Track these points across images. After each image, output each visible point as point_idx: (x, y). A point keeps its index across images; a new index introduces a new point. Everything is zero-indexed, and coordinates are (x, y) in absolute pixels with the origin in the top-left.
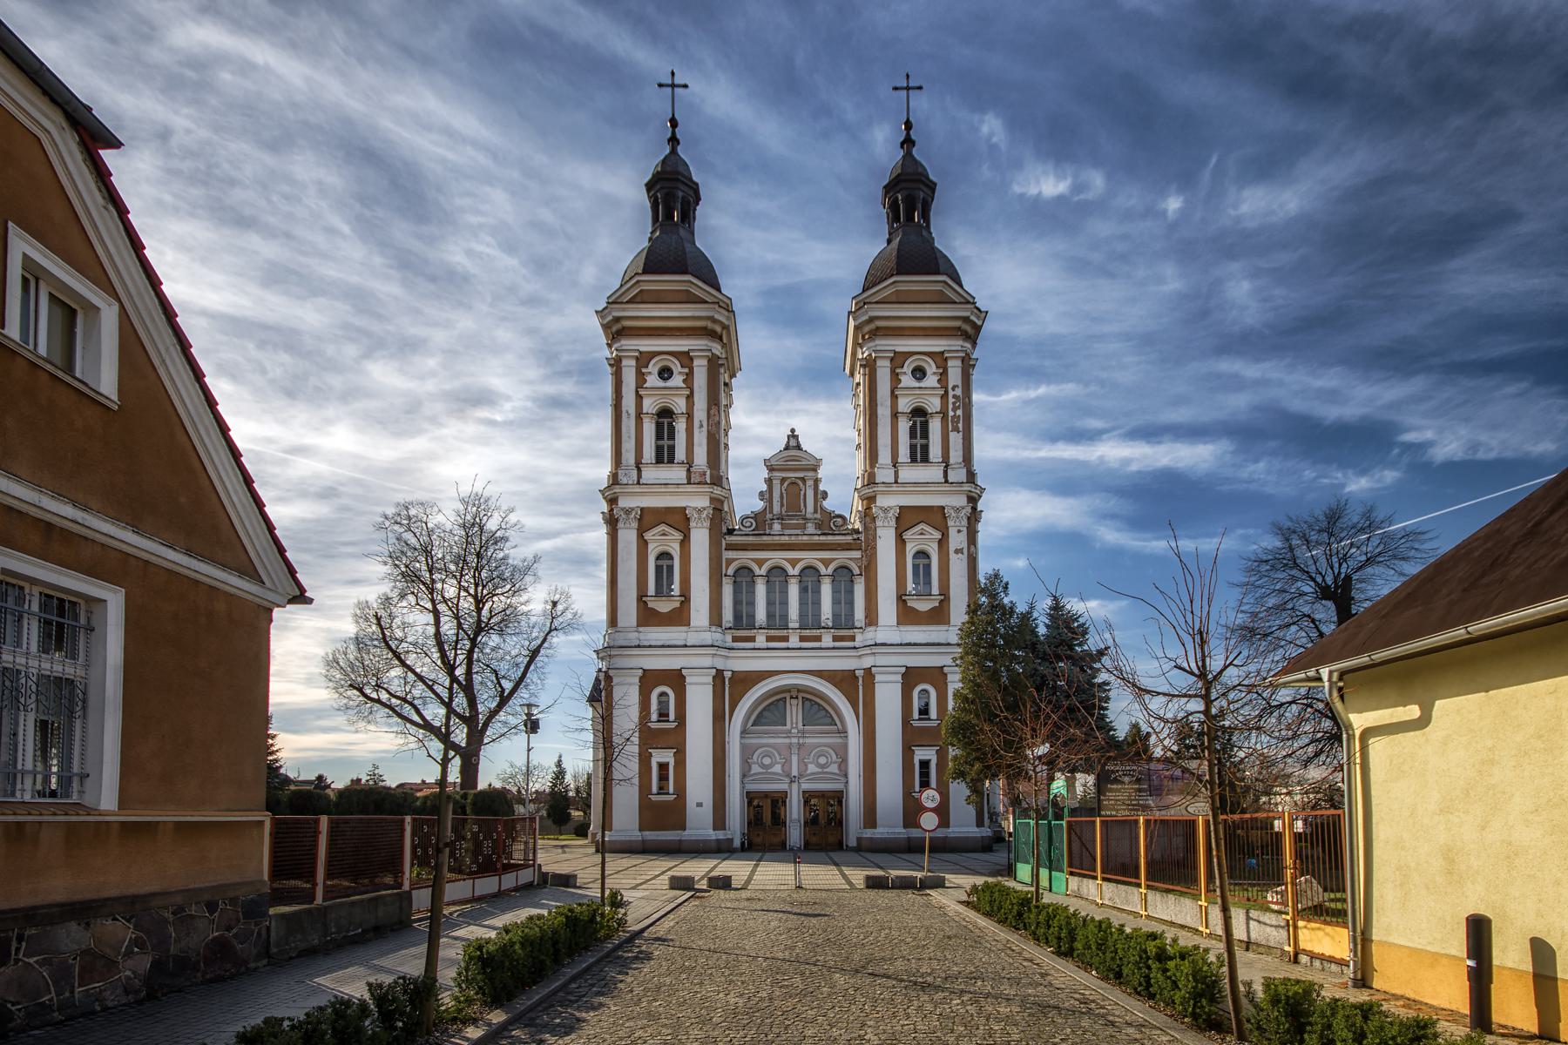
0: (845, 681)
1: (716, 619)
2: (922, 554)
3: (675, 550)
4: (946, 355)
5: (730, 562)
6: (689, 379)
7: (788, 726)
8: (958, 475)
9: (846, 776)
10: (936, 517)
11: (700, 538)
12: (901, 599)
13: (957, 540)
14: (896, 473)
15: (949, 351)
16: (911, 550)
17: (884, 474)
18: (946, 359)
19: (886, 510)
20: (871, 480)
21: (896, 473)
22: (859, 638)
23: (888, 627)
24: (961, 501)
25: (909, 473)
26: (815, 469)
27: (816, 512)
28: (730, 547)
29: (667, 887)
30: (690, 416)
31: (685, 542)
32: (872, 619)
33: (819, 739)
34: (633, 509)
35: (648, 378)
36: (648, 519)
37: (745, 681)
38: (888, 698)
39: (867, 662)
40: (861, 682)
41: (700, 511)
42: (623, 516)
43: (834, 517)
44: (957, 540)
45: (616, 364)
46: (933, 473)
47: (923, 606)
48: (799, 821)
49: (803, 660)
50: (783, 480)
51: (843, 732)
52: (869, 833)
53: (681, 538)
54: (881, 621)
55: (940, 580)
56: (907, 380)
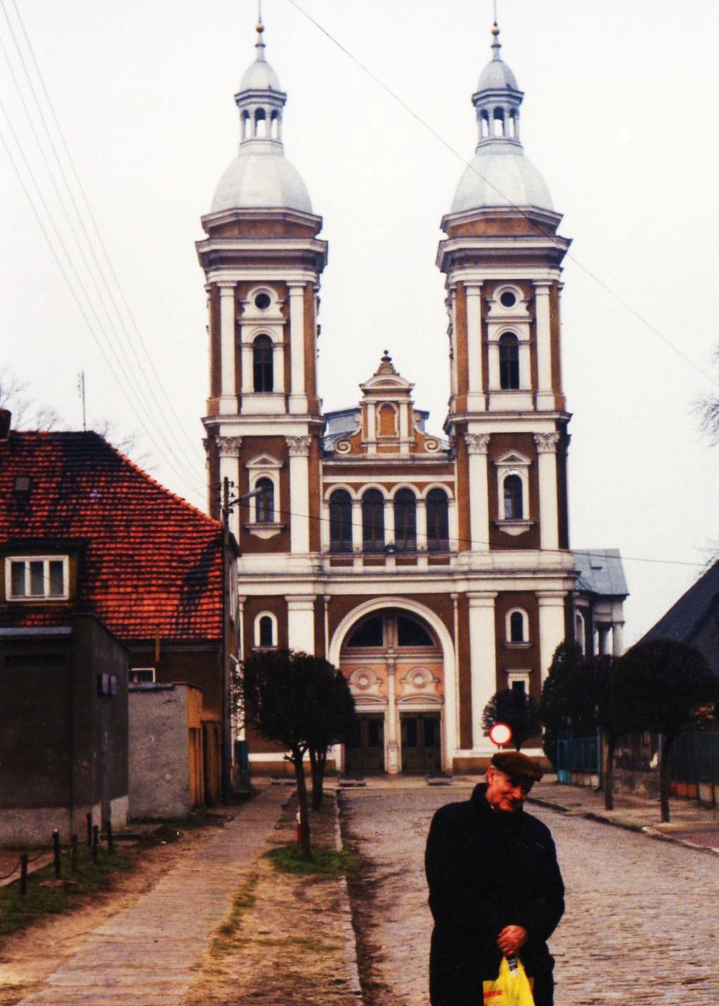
0: (440, 603)
1: (314, 544)
2: (265, 483)
3: (275, 478)
4: (465, 284)
5: (327, 486)
6: (285, 307)
7: (385, 646)
8: (546, 402)
9: (442, 697)
10: (527, 444)
11: (299, 467)
12: (494, 526)
13: (547, 464)
14: (240, 405)
15: (468, 281)
16: (502, 475)
17: (475, 403)
18: (466, 288)
19: (477, 437)
20: (214, 410)
21: (240, 405)
22: (453, 561)
23: (481, 554)
24: (550, 428)
25: (255, 404)
26: (407, 392)
27: (410, 435)
28: (328, 470)
29: (660, 819)
30: (287, 347)
31: (285, 470)
32: (466, 541)
33: (411, 659)
34: (482, 435)
35: (246, 307)
36: (248, 447)
37: (345, 604)
38: (482, 622)
39: (462, 587)
40: (456, 604)
41: (299, 440)
42: (225, 445)
43: (427, 440)
44: (547, 464)
45: (214, 292)
46: (272, 404)
47: (515, 531)
48: (396, 743)
49: (384, 585)
50: (377, 404)
51: (439, 653)
52: (466, 754)
53: (281, 466)
54: (474, 546)
55: (282, 504)
56: (251, 310)
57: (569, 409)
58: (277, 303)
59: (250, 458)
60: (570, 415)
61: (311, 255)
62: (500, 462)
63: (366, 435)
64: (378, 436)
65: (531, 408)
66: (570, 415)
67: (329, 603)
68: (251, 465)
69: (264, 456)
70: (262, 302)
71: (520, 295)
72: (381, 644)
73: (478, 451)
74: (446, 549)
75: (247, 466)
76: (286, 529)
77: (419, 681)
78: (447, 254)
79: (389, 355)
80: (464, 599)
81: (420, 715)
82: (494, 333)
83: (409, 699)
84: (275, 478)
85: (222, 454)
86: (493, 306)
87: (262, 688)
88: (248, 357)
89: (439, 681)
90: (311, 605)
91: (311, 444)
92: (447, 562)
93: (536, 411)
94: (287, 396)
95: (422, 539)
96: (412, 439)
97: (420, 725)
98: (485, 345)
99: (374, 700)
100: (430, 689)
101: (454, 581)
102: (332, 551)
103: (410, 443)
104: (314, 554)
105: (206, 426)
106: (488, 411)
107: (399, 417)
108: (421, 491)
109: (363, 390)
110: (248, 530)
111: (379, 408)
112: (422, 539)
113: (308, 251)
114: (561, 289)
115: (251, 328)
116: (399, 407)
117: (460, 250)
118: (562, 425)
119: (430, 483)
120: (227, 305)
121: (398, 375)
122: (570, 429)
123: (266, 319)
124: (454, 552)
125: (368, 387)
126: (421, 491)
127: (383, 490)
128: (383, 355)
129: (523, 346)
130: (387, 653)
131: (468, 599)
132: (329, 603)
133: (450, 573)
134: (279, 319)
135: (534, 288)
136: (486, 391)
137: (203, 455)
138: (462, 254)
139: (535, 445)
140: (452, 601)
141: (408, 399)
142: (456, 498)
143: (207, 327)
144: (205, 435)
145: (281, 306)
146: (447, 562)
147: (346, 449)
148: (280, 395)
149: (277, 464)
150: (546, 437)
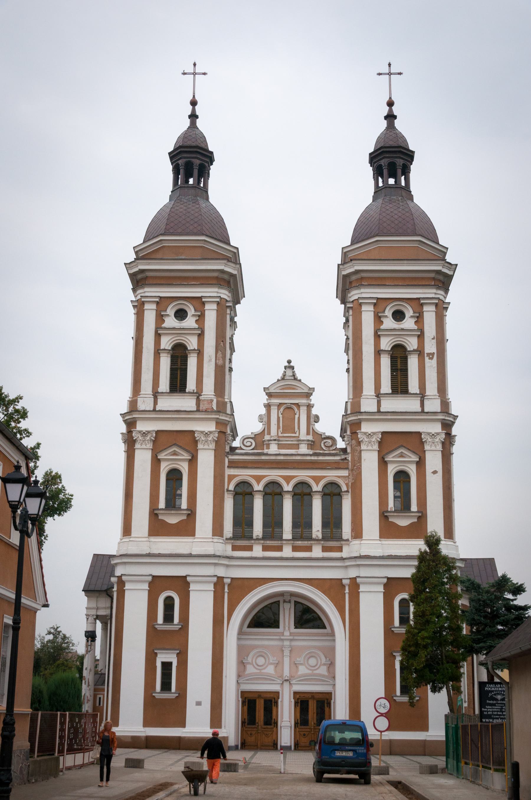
3: (184, 468)
5: (231, 478)
14: (155, 403)
19: (369, 435)
21: (155, 403)
22: (345, 548)
24: (437, 428)
25: (388, 405)
26: (308, 395)
27: (308, 433)
28: (233, 465)
30: (200, 352)
31: (193, 462)
32: (357, 533)
39: (353, 573)
41: (207, 434)
43: (324, 438)
46: (412, 405)
50: (280, 405)
54: (365, 535)
57: (454, 411)
58: (412, 317)
59: (388, 453)
60: (456, 417)
61: (226, 277)
62: (389, 458)
63: (269, 433)
64: (280, 435)
65: (420, 410)
66: (456, 417)
67: (229, 585)
68: (389, 458)
69: (175, 449)
70: (399, 316)
71: (409, 312)
72: (278, 627)
73: (370, 448)
74: (340, 538)
75: (386, 459)
76: (191, 514)
77: (312, 661)
78: (345, 277)
79: (292, 364)
80: (355, 584)
81: (313, 695)
82: (166, 343)
83: (306, 679)
84: (184, 468)
85: (137, 446)
86: (167, 319)
87: (405, 662)
88: (165, 362)
89: (331, 665)
90: (211, 587)
91: (218, 438)
92: (340, 549)
93: (379, 411)
94: (422, 396)
95: (258, 529)
96: (310, 437)
97: (312, 707)
98: (157, 352)
99: (266, 679)
100: (323, 670)
101: (346, 567)
102: (235, 537)
103: (308, 440)
104: (216, 539)
105: (125, 421)
106: (154, 410)
107: (299, 418)
108: (258, 483)
109: (267, 394)
110: (157, 515)
111: (282, 410)
112: (258, 529)
113: (222, 271)
114: (446, 308)
115: (169, 337)
116: (299, 410)
117: (357, 272)
118: (447, 426)
119: (238, 475)
120: (150, 317)
121: (300, 381)
122: (455, 431)
123: (403, 330)
124: (347, 540)
125: (272, 390)
126: (288, 483)
127: (253, 482)
128: (287, 364)
129: (192, 355)
130: (283, 635)
131: (357, 586)
132: (229, 585)
133: (342, 559)
134: (194, 329)
135: (204, 303)
136: (378, 395)
137: (122, 447)
138: (358, 276)
139: (422, 443)
140: (344, 586)
141: (309, 401)
142: (350, 490)
143: (133, 338)
144: (124, 428)
145: (197, 318)
146: (340, 549)
147: (250, 446)
148: (192, 393)
149: (187, 456)
150: (433, 436)
